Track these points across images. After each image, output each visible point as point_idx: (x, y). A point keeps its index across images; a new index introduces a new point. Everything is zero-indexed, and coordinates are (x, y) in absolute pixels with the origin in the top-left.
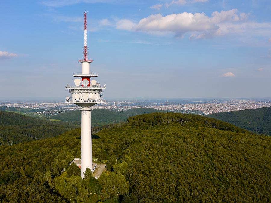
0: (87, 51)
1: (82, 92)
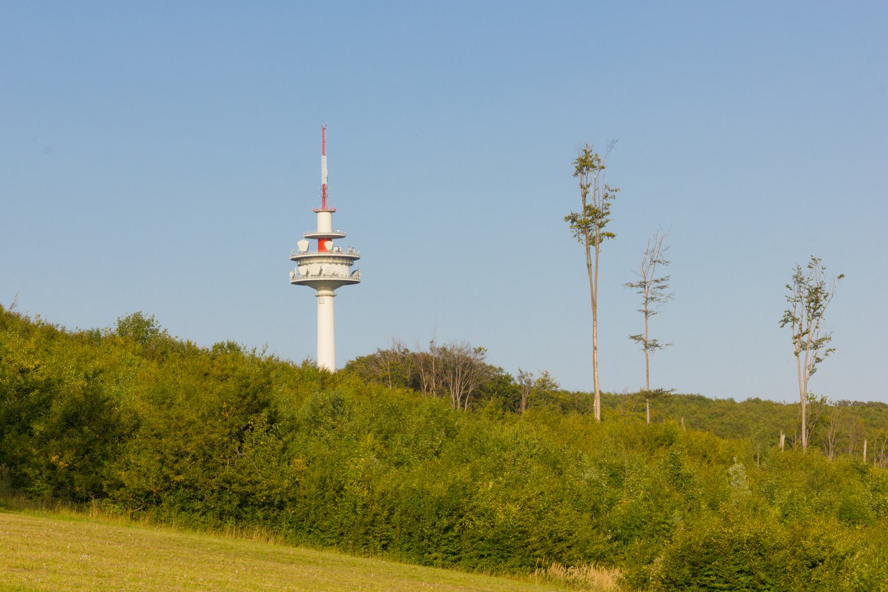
1: (312, 261)
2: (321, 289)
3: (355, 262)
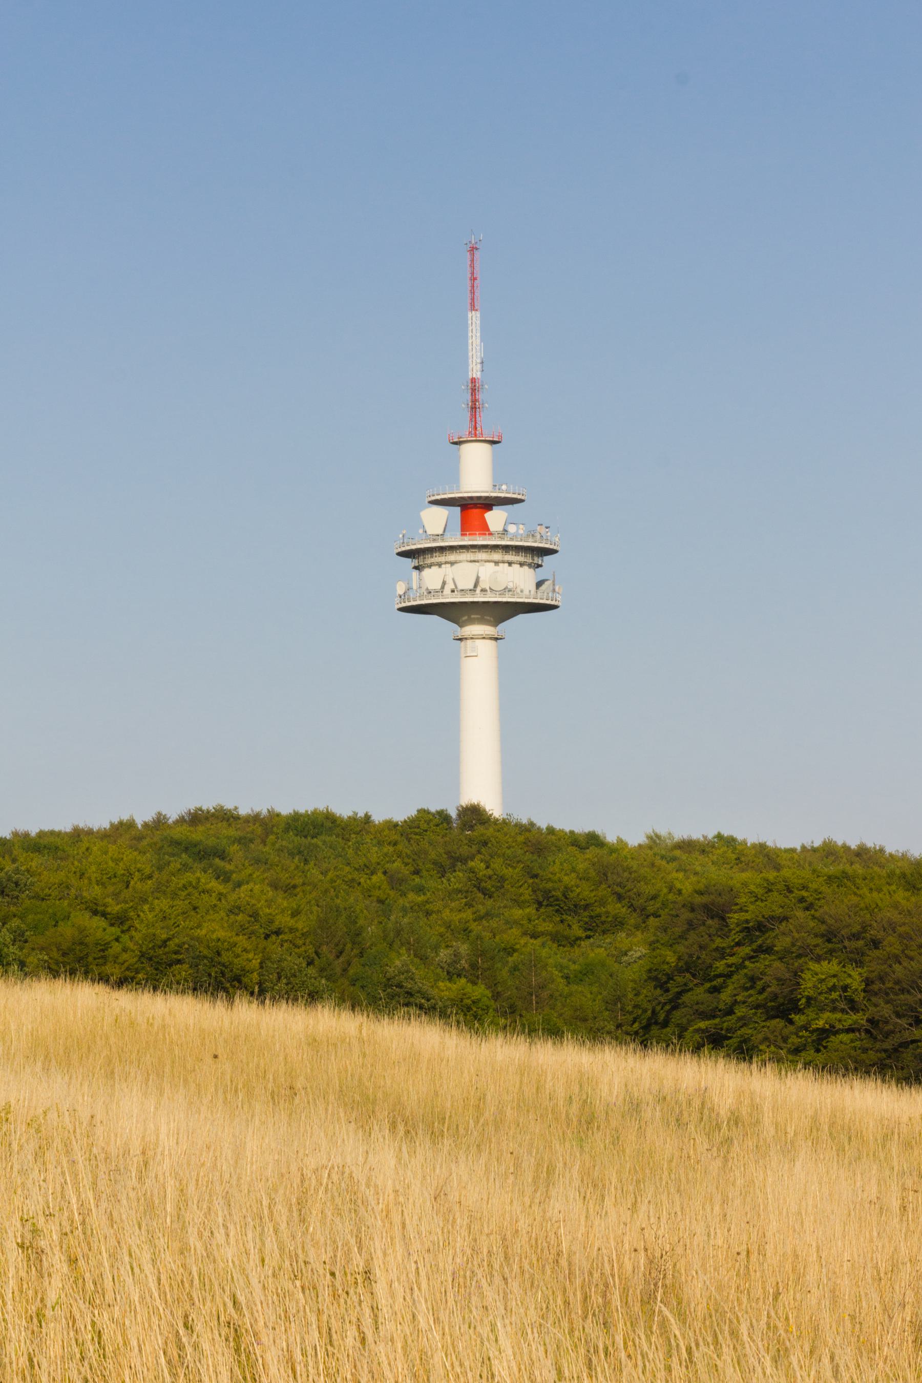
0: (480, 396)
1: (452, 557)
2: (471, 622)
3: (547, 559)
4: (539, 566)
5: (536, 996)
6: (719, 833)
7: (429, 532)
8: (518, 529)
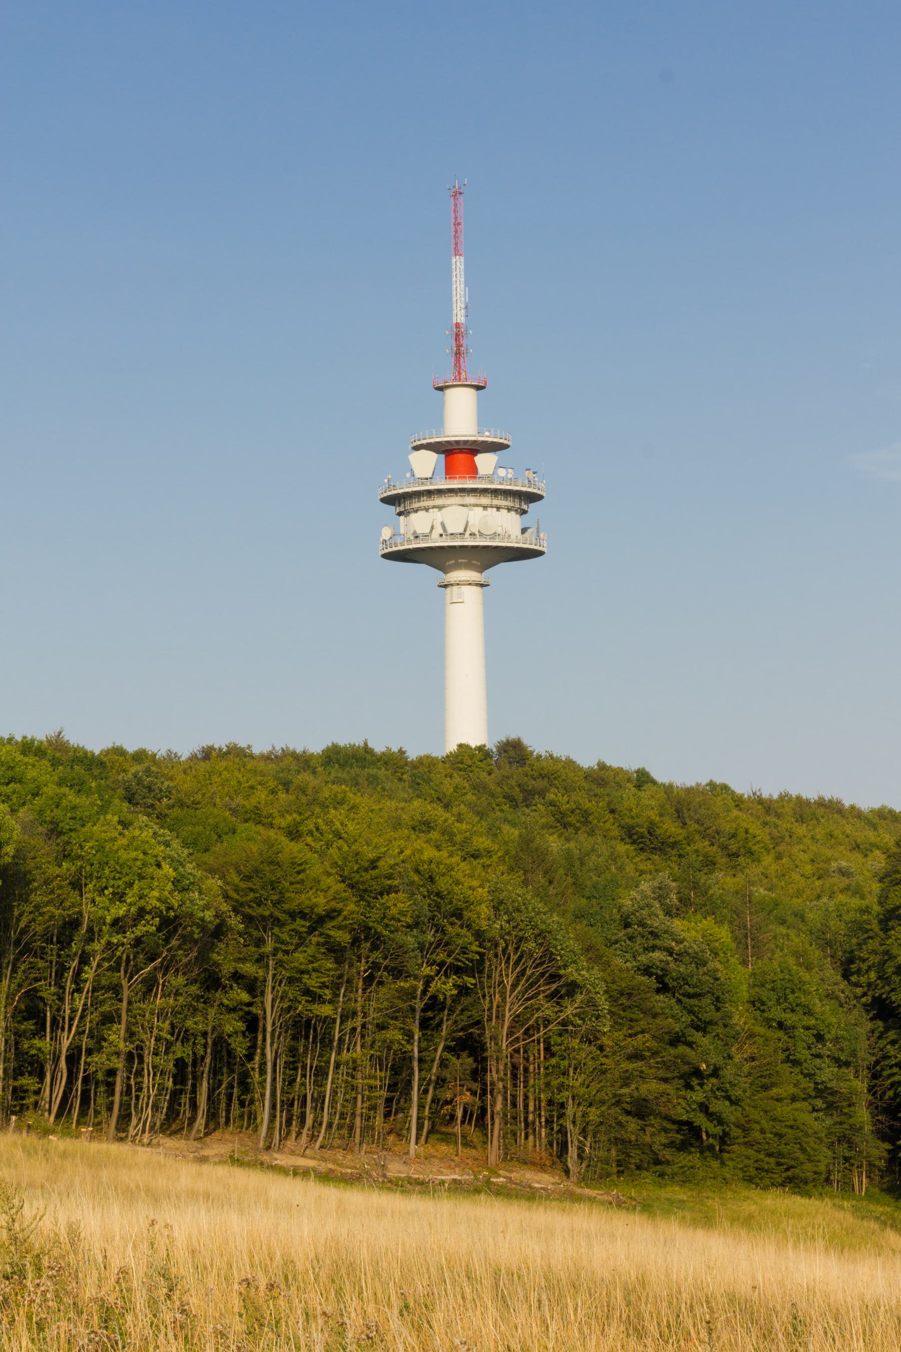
0: (464, 342)
1: (439, 501)
2: (458, 567)
4: (524, 512)
5: (752, 939)
6: (711, 781)
7: (417, 475)
8: (507, 473)
